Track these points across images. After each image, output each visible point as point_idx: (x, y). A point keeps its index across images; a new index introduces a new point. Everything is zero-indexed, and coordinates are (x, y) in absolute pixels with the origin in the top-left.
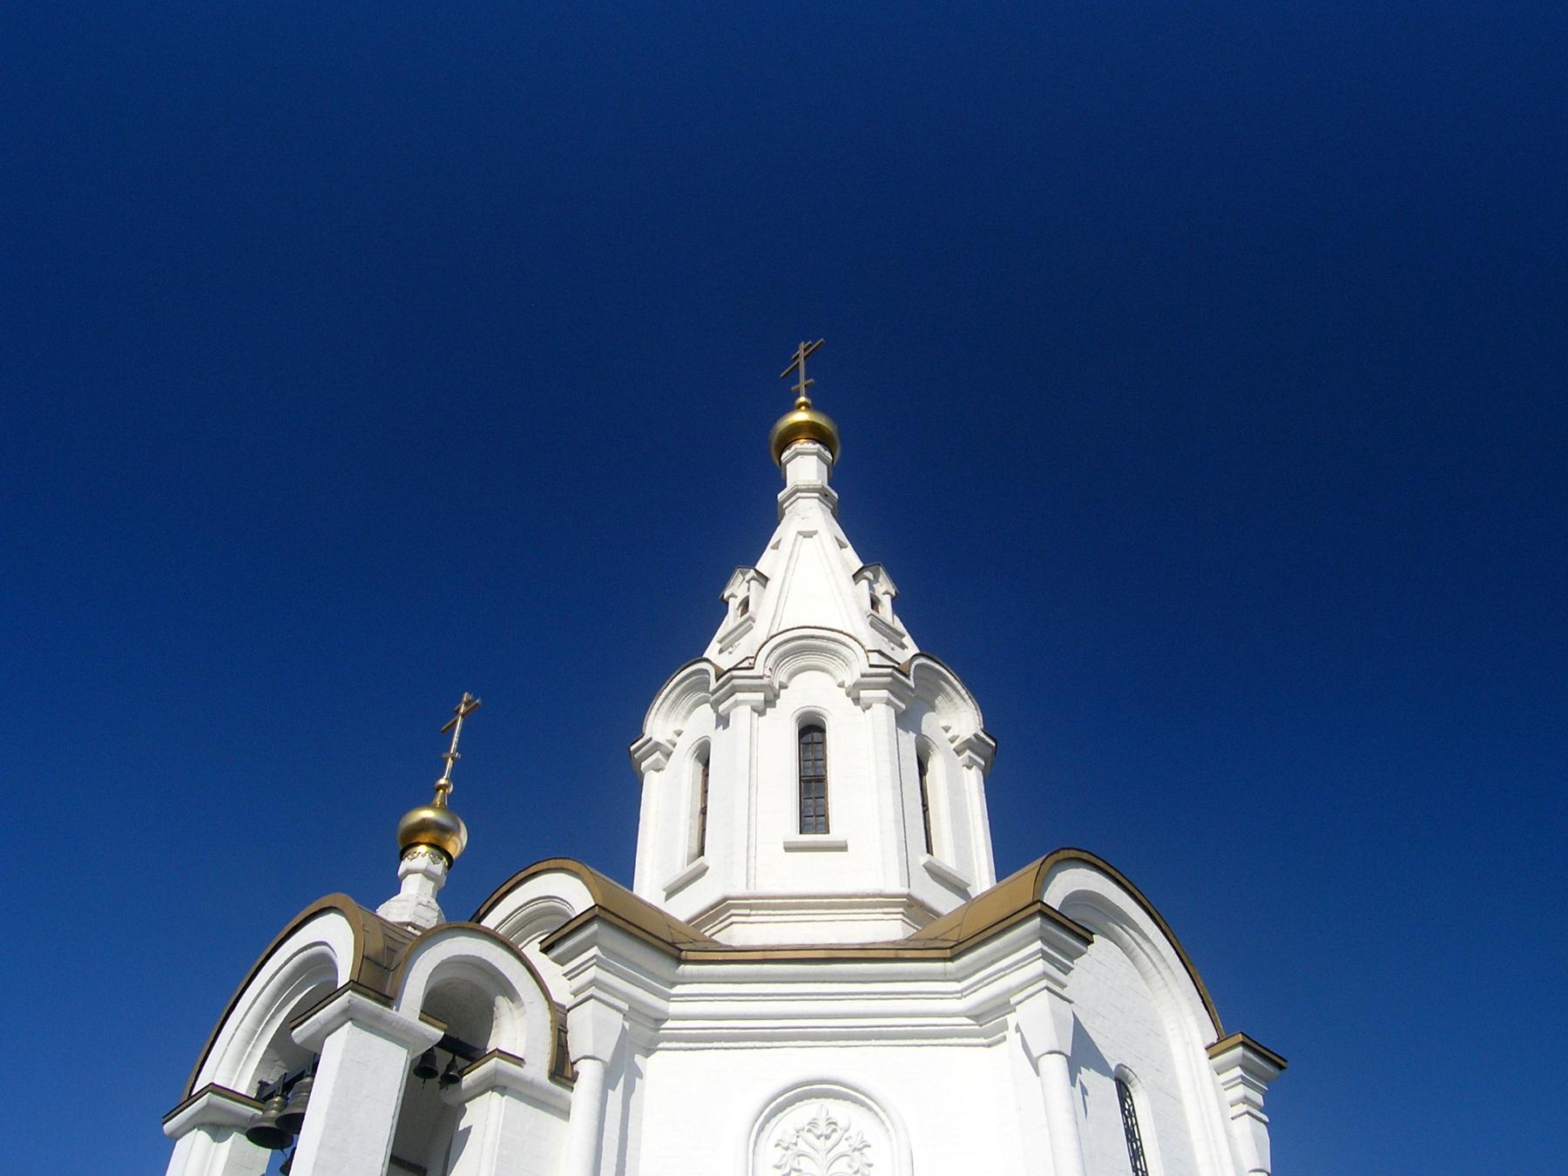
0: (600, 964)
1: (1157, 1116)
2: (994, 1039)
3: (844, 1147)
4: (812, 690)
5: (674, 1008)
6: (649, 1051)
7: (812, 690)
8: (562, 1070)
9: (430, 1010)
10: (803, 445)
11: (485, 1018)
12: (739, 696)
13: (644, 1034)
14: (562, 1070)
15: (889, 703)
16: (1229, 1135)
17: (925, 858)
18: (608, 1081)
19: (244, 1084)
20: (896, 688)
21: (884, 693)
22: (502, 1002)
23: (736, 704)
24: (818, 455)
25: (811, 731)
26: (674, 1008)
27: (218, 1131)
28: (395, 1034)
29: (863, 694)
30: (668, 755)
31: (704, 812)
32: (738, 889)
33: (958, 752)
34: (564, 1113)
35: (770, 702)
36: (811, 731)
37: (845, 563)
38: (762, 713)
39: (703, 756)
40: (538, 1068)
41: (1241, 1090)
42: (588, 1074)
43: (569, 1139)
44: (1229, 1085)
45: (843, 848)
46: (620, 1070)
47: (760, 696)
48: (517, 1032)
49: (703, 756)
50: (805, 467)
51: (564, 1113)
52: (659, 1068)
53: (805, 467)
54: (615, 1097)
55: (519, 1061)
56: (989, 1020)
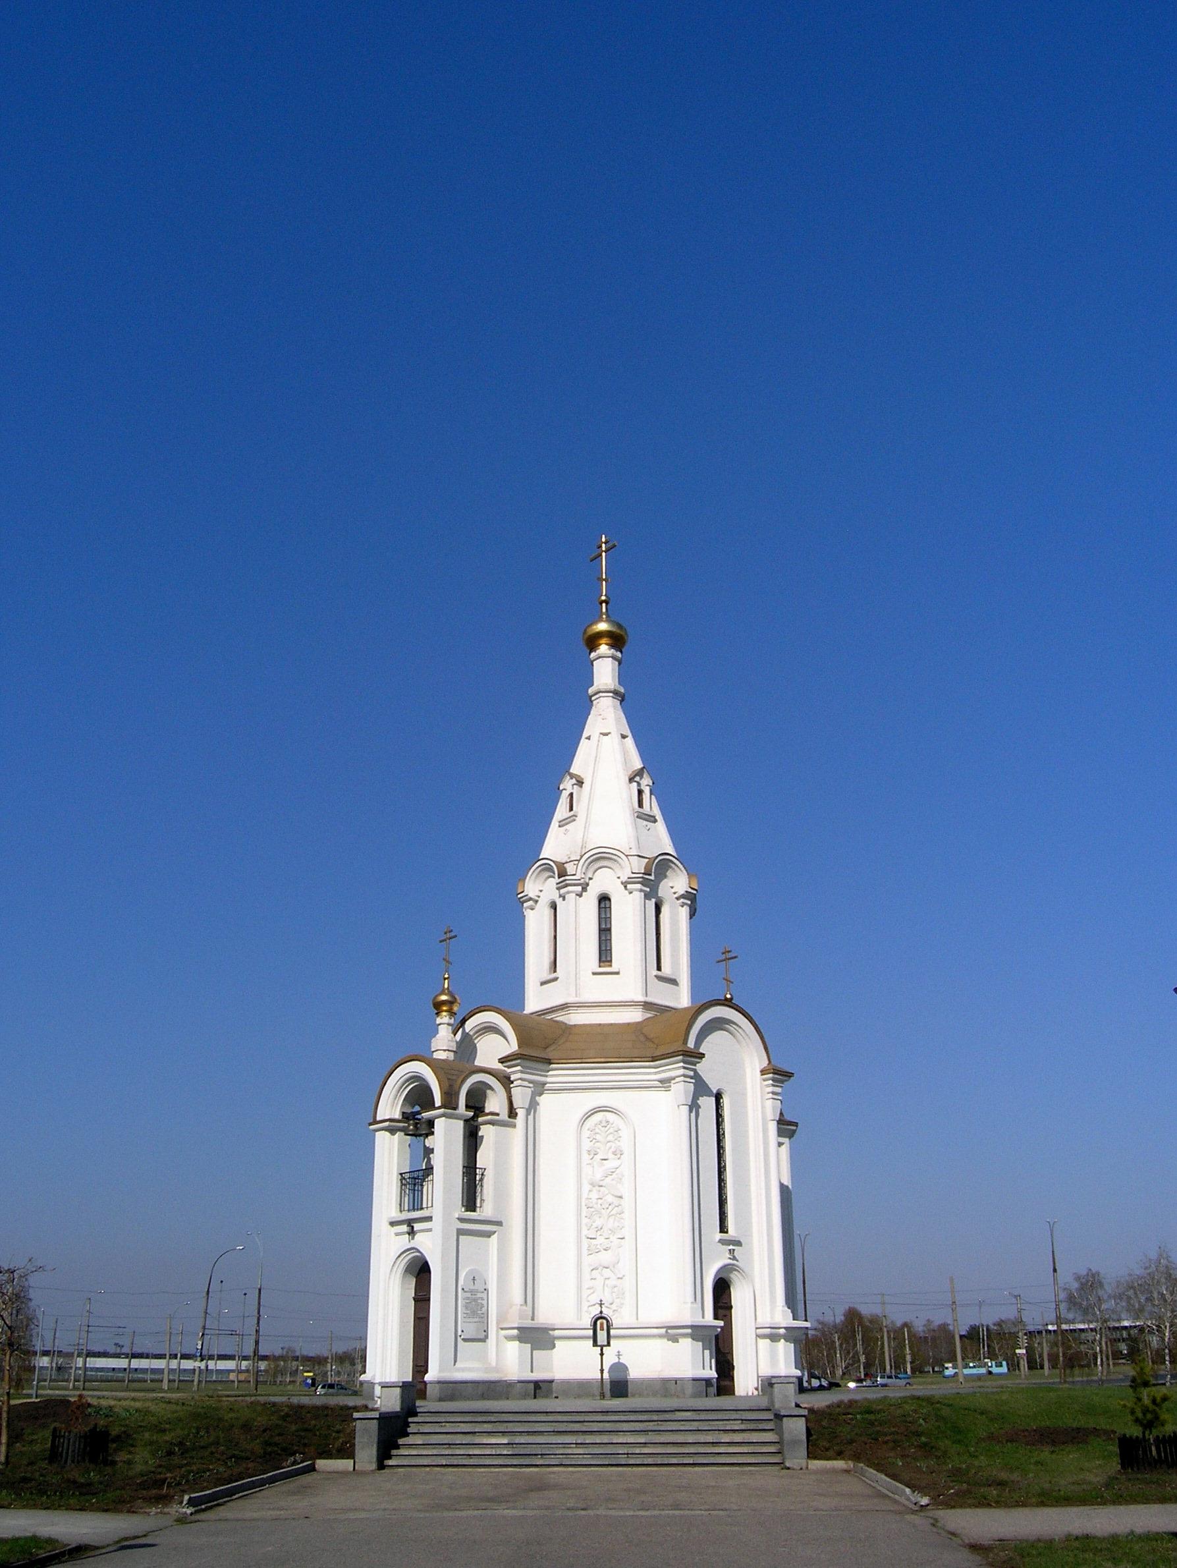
0: (522, 1072)
1: (732, 1106)
2: (668, 1089)
3: (611, 1130)
4: (605, 880)
5: (549, 1079)
6: (541, 1094)
7: (605, 880)
8: (512, 1113)
9: (468, 1107)
10: (604, 641)
11: (484, 1097)
12: (570, 888)
13: (540, 1089)
14: (512, 1113)
15: (641, 890)
16: (763, 1107)
17: (656, 973)
18: (528, 1113)
19: (397, 1115)
20: (645, 882)
21: (639, 886)
22: (489, 1092)
23: (568, 892)
24: (614, 657)
25: (604, 899)
26: (549, 1079)
27: (392, 1131)
28: (457, 1117)
29: (629, 886)
30: (536, 902)
31: (555, 937)
32: (571, 999)
33: (677, 899)
34: (515, 1126)
35: (584, 889)
36: (604, 899)
37: (626, 760)
38: (580, 896)
39: (554, 906)
40: (504, 1115)
41: (771, 1089)
42: (521, 1113)
43: (517, 1135)
44: (768, 1086)
45: (618, 973)
46: (533, 1107)
47: (579, 888)
48: (495, 1103)
49: (554, 906)
50: (605, 670)
51: (515, 1126)
52: (544, 1100)
53: (605, 670)
54: (531, 1118)
55: (498, 1115)
56: (665, 1083)
